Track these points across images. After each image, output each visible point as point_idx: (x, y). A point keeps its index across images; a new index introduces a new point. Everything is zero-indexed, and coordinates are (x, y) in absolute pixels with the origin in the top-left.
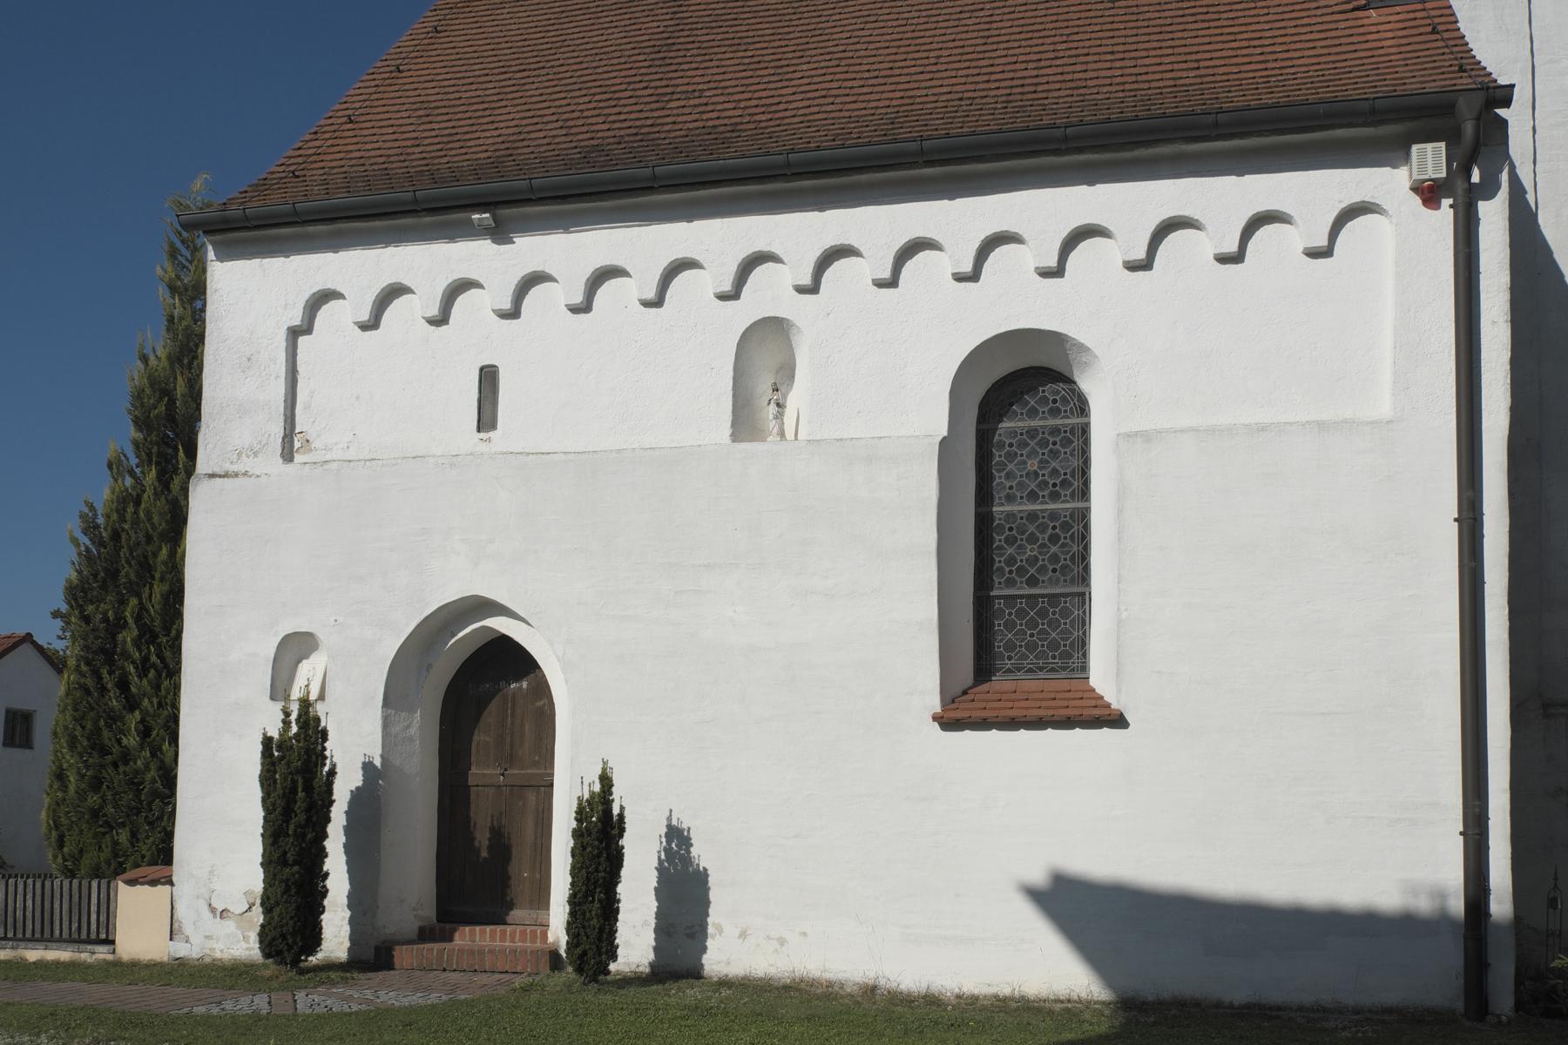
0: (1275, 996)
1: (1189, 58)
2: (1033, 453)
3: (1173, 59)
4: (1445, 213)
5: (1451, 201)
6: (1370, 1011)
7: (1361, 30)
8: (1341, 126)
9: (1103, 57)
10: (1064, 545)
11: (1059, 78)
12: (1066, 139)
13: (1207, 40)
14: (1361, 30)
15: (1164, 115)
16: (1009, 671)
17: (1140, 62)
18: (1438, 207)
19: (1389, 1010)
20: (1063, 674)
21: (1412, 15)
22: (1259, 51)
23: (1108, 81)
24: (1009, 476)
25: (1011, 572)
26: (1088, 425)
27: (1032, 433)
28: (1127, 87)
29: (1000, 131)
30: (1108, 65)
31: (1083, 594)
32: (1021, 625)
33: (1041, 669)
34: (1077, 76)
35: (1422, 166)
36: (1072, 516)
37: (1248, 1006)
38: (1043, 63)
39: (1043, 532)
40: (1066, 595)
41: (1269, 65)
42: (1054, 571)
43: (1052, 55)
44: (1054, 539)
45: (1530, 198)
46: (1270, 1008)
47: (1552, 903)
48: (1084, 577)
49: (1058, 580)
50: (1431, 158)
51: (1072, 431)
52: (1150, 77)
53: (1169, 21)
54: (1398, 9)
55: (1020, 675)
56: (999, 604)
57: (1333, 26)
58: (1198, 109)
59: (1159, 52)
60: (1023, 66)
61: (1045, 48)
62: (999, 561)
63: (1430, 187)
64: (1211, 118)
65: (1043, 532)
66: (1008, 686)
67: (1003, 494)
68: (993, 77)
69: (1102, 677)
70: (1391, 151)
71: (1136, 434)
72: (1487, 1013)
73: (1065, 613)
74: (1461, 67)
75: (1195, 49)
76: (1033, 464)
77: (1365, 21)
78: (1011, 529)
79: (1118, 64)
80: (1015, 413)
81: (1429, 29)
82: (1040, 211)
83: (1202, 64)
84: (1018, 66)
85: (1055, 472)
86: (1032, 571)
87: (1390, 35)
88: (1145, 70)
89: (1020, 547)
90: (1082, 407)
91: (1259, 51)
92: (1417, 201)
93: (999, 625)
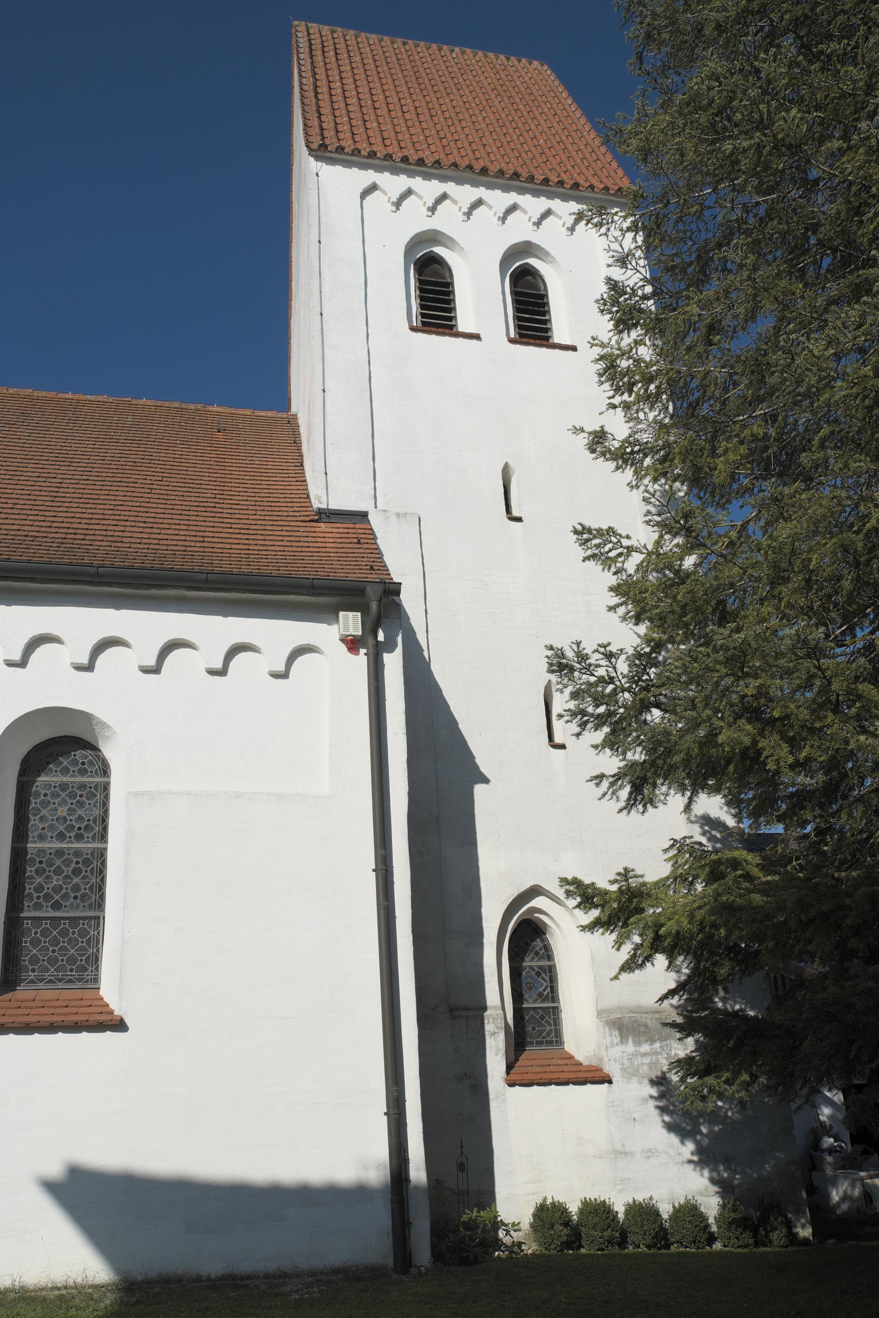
0: (245, 1267)
1: (198, 534)
2: (64, 802)
3: (187, 533)
4: (361, 660)
5: (365, 651)
6: (322, 1273)
7: (314, 535)
8: (293, 593)
9: (138, 524)
10: (85, 877)
11: (104, 533)
12: (97, 575)
13: (212, 524)
14: (314, 535)
15: (172, 569)
16: (32, 981)
17: (163, 531)
18: (358, 654)
19: (335, 1271)
20: (79, 985)
21: (346, 531)
22: (246, 537)
23: (139, 541)
24: (42, 819)
25: (38, 898)
26: (108, 783)
27: (64, 786)
28: (152, 546)
29: (50, 563)
30: (141, 530)
31: (99, 918)
32: (44, 942)
33: (60, 980)
34: (116, 534)
35: (346, 627)
36: (92, 854)
37: (223, 1278)
38: (93, 521)
39: (68, 866)
40: (84, 918)
41: (251, 547)
42: (75, 898)
43: (101, 517)
44: (76, 872)
45: (426, 654)
46: (242, 1278)
47: (461, 1167)
48: (100, 904)
49: (78, 906)
50: (351, 622)
51: (96, 787)
52: (168, 542)
53: (188, 508)
54: (339, 525)
55: (41, 985)
56: (28, 924)
57: (297, 529)
58: (197, 569)
59: (178, 527)
60: (79, 521)
61: (97, 511)
62: (29, 888)
63: (351, 640)
64: (203, 576)
65: (68, 866)
66: (30, 995)
67: (36, 834)
68: (55, 525)
69: (110, 990)
70: (326, 613)
71: (143, 793)
72: (411, 1266)
73: (84, 933)
74: (372, 567)
75: (203, 529)
76: (62, 811)
77: (317, 530)
78: (41, 862)
79: (148, 530)
80: (51, 769)
81: (356, 540)
82: (79, 623)
83: (206, 539)
84: (74, 520)
85: (80, 818)
86: (57, 898)
87: (332, 540)
88: (166, 537)
89: (48, 877)
90: (105, 770)
91: (246, 537)
92: (343, 648)
93: (26, 942)
